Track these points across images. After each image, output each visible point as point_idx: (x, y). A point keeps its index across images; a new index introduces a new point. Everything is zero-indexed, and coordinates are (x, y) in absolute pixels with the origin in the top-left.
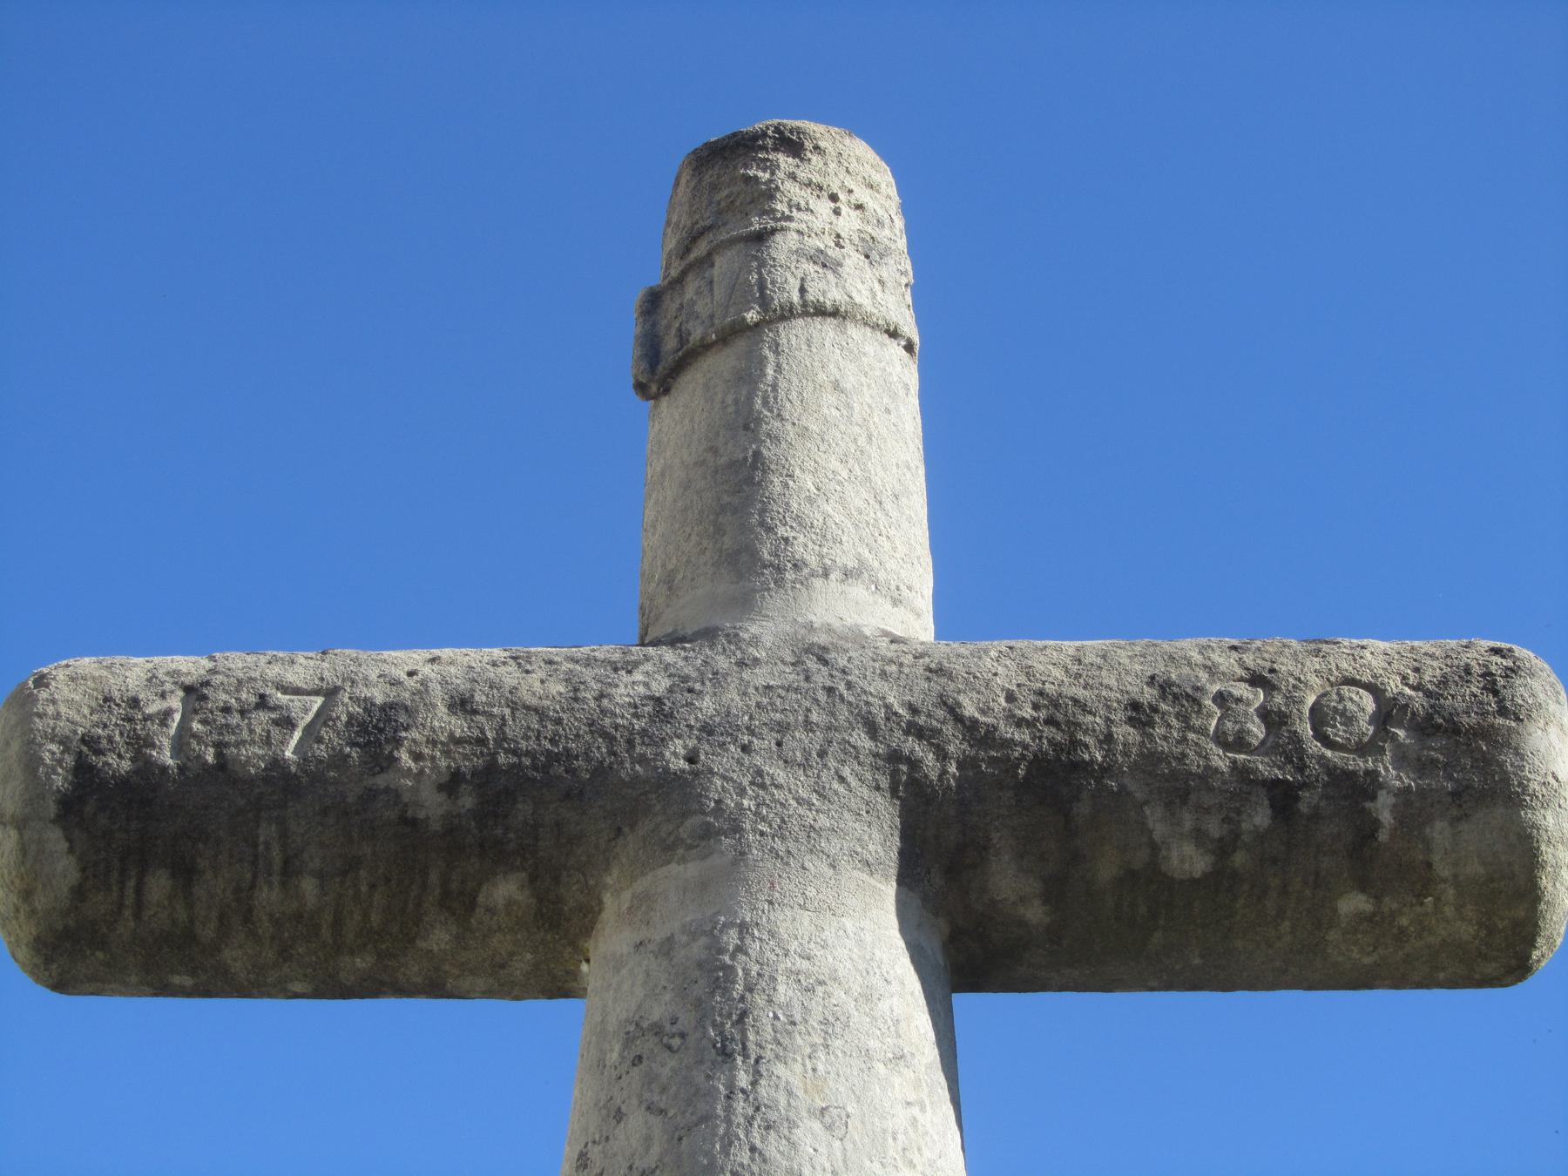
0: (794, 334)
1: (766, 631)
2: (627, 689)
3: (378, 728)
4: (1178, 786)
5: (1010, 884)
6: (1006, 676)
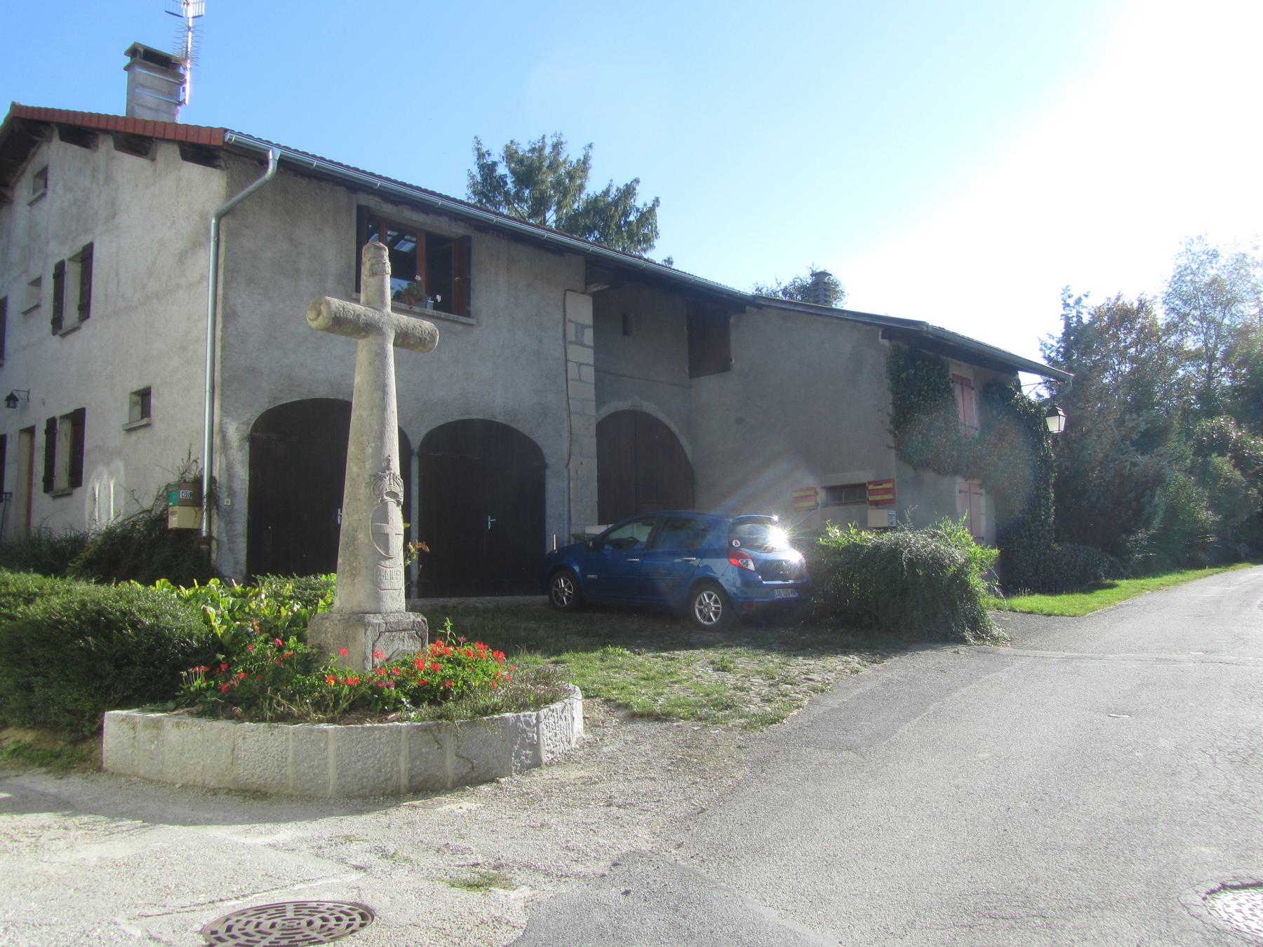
4: (414, 336)
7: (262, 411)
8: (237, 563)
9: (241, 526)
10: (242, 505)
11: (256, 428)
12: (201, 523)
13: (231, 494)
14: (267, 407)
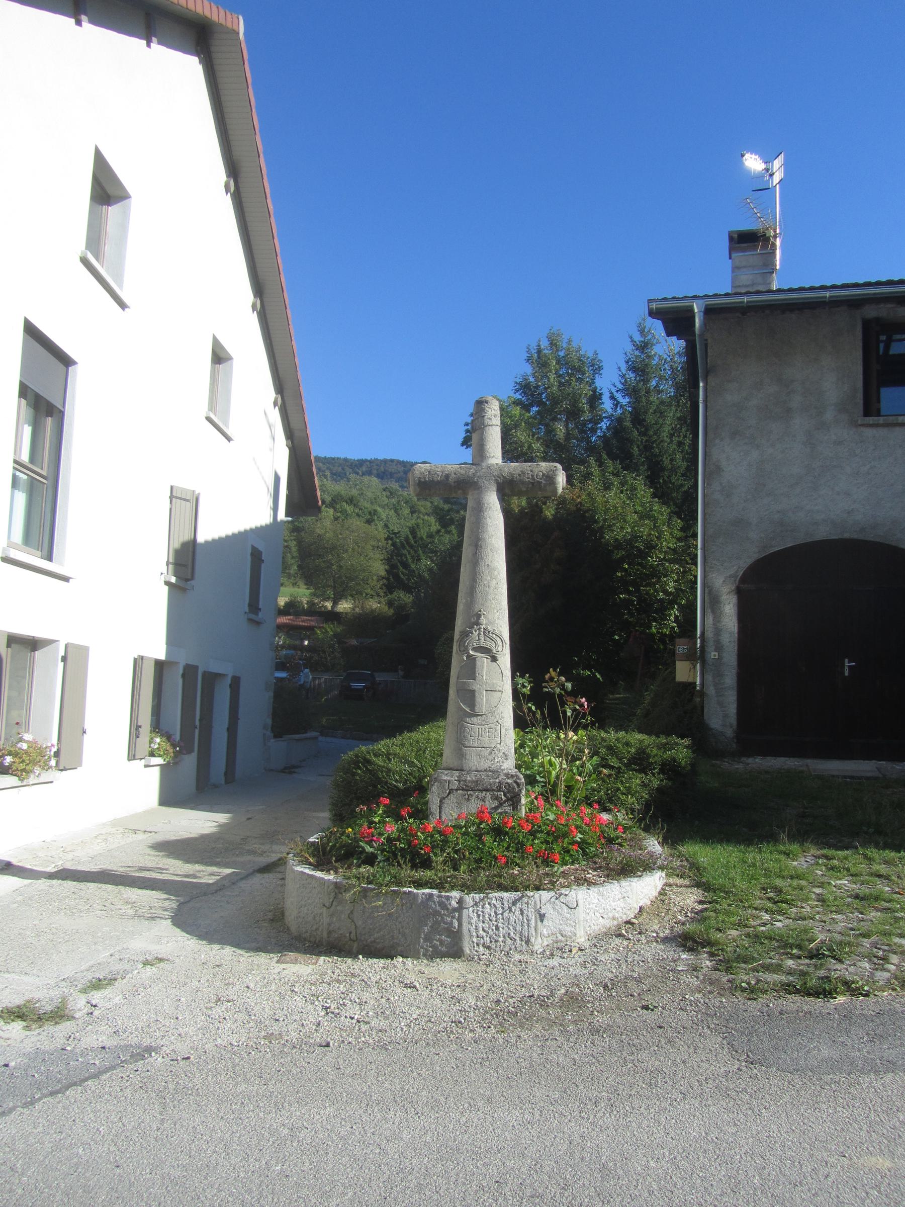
0: (487, 428)
1: (484, 464)
2: (472, 471)
3: (447, 476)
4: (523, 483)
5: (507, 491)
6: (506, 470)
7: (750, 561)
8: (726, 716)
9: (730, 679)
10: (731, 656)
11: (744, 579)
12: (695, 677)
13: (719, 648)
14: (756, 556)
